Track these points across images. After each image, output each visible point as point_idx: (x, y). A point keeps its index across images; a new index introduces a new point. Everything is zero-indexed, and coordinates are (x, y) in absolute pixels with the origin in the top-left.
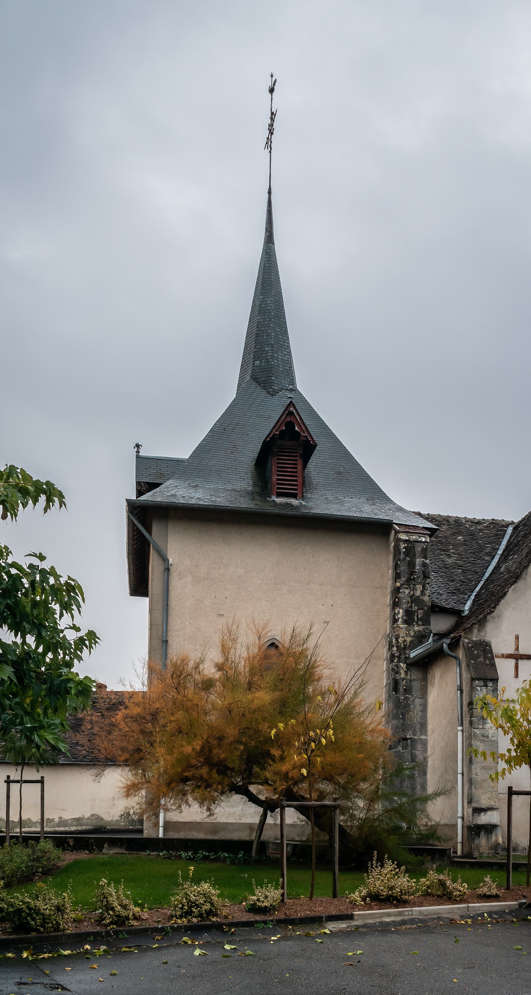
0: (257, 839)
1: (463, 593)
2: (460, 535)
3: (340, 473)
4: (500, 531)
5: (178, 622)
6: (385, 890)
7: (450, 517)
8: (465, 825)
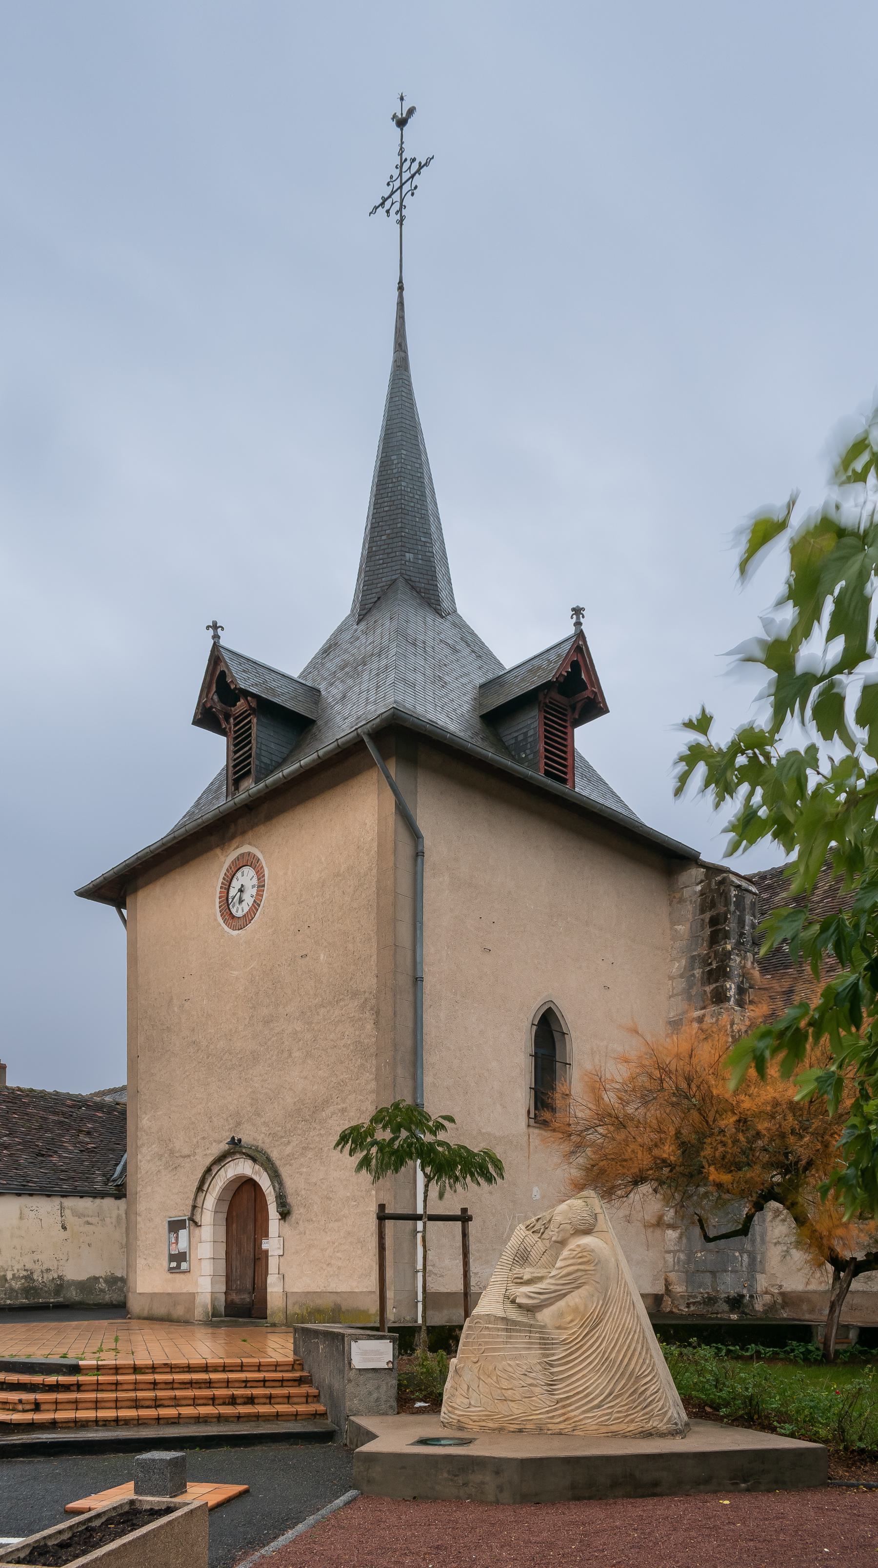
5: (432, 950)
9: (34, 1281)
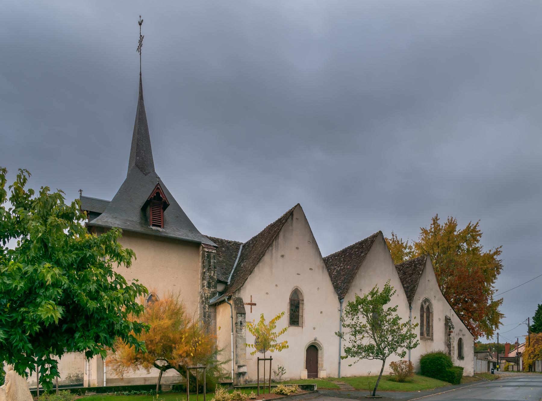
0: (158, 383)
1: (227, 274)
2: (223, 248)
3: (177, 217)
4: (238, 247)
6: (222, 399)
7: (219, 239)
8: (235, 373)
9: (79, 377)
